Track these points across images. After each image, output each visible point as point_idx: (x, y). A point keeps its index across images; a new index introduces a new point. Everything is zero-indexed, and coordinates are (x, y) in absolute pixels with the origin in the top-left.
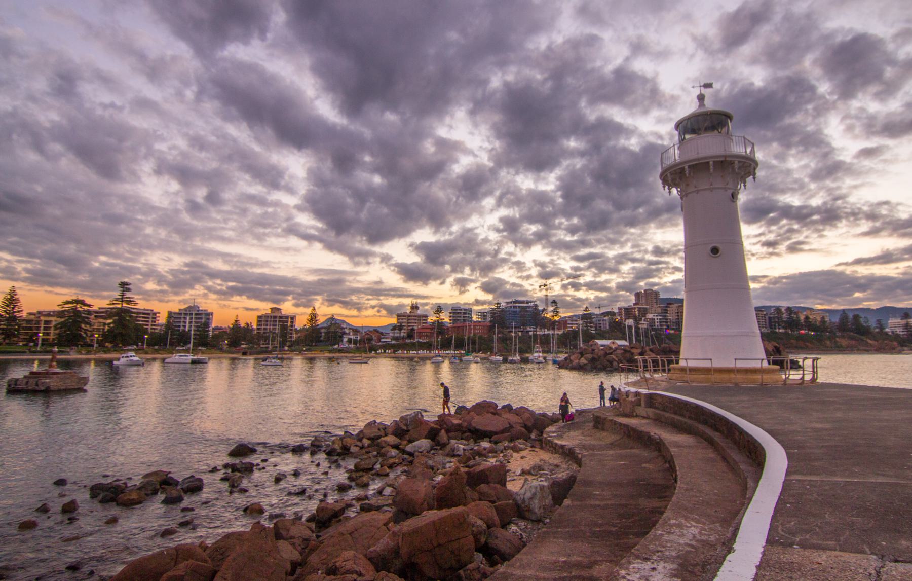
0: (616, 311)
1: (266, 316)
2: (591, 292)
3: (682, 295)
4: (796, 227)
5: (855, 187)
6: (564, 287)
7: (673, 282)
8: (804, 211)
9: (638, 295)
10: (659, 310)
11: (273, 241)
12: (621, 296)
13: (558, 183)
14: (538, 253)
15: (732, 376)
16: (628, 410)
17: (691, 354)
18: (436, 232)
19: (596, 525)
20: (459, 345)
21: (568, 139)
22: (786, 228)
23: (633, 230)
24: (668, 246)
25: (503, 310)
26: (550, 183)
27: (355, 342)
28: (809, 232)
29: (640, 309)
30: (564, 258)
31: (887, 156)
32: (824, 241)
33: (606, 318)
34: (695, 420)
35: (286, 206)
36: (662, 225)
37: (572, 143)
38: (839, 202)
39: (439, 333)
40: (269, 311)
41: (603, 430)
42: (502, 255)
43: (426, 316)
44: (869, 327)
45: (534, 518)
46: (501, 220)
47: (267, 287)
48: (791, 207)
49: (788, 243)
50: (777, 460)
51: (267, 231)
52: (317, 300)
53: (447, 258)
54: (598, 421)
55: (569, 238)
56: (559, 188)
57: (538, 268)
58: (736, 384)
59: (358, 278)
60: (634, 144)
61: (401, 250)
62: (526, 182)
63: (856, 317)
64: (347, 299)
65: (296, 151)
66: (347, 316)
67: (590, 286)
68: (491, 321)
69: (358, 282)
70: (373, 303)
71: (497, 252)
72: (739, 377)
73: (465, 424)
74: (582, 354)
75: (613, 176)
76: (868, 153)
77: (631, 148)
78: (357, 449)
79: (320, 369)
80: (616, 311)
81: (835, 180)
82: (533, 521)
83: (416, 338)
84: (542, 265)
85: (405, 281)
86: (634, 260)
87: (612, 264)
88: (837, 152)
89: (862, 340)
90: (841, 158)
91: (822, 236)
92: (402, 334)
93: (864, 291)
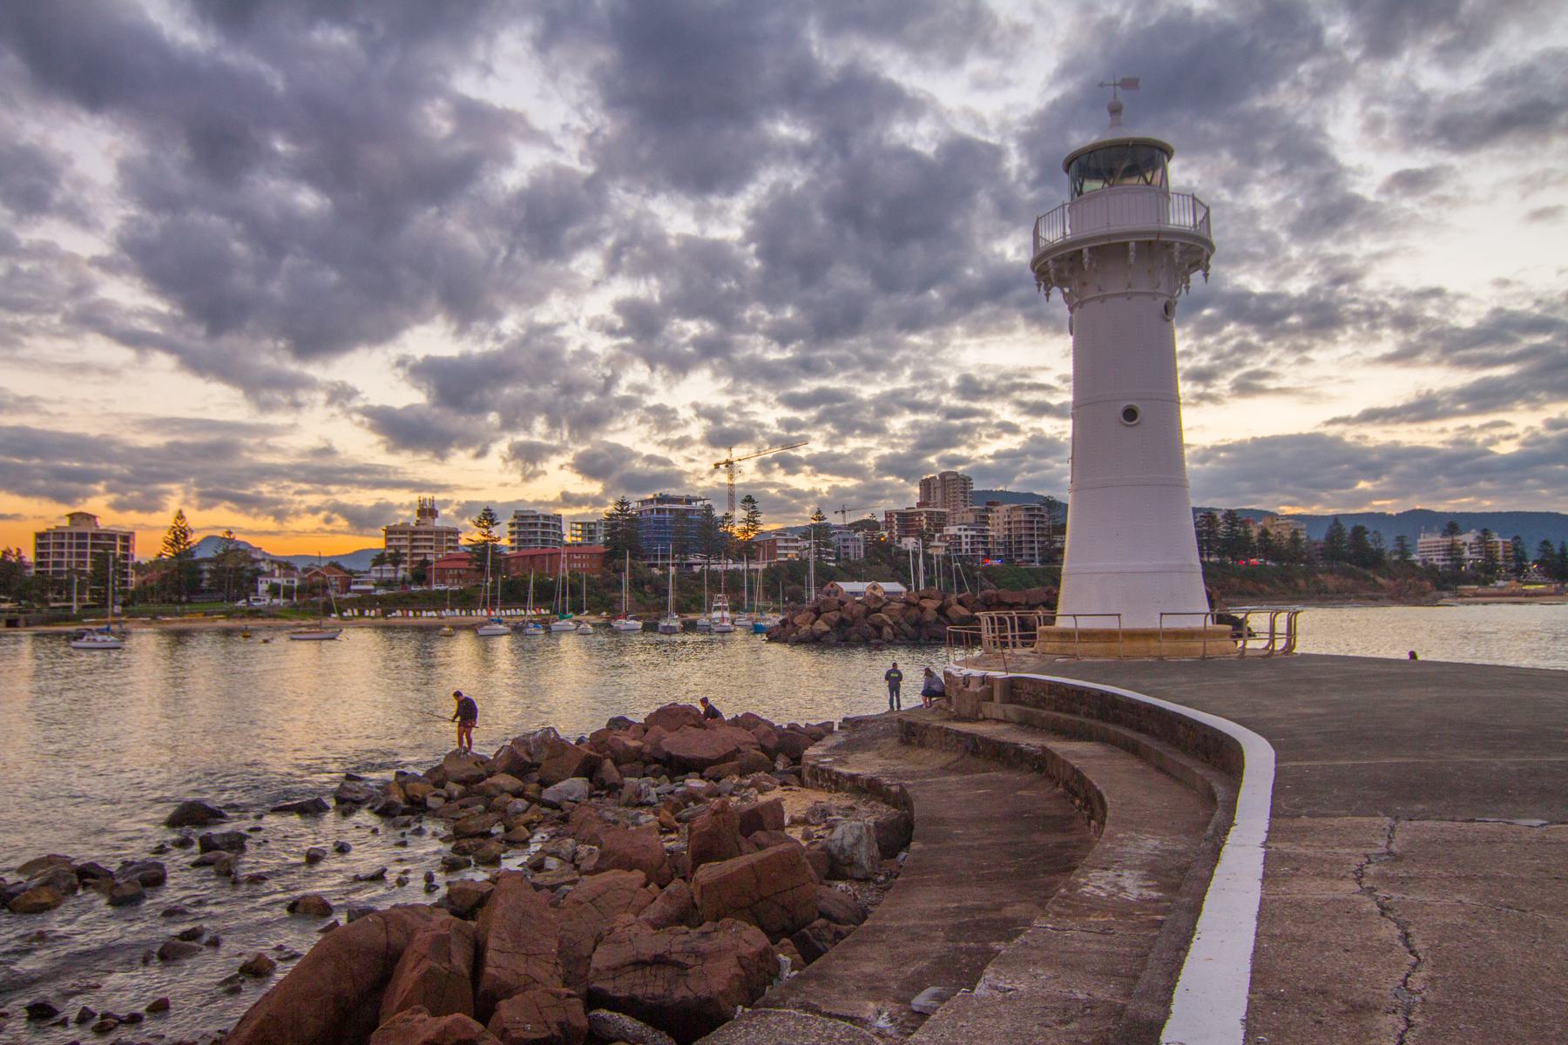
0: (881, 519)
1: (59, 533)
2: (822, 476)
3: (1065, 496)
4: (1254, 339)
5: (1379, 256)
6: (764, 466)
7: (998, 455)
8: (1274, 306)
9: (926, 485)
10: (971, 518)
11: (40, 346)
12: (886, 485)
13: (751, 223)
14: (702, 388)
15: (1153, 644)
16: (966, 710)
17: (1081, 604)
18: (461, 332)
19: (982, 868)
20: (545, 594)
21: (772, 116)
22: (1233, 342)
23: (915, 339)
24: (990, 377)
25: (633, 519)
26: (730, 222)
27: (289, 593)
28: (1281, 350)
29: (930, 515)
30: (764, 401)
31: (1448, 190)
32: (1309, 372)
33: (860, 535)
34: (1099, 718)
35: (70, 260)
36: (978, 330)
37: (785, 129)
38: (1343, 288)
39: (496, 571)
40: (66, 523)
41: (922, 745)
42: (621, 391)
43: (456, 532)
44: (1380, 552)
45: (859, 874)
46: (623, 307)
47: (36, 461)
48: (1249, 295)
49: (1235, 374)
50: (1259, 756)
51: (22, 319)
52: (170, 493)
53: (488, 394)
54: (909, 732)
55: (774, 355)
56: (751, 236)
57: (705, 422)
58: (1161, 658)
59: (272, 441)
60: (920, 137)
61: (377, 374)
62: (675, 219)
63: (1358, 532)
64: (250, 492)
65: (84, 116)
66: (250, 533)
67: (821, 464)
68: (607, 544)
69: (272, 449)
70: (314, 500)
71: (610, 382)
72: (1166, 645)
73: (647, 749)
74: (818, 613)
75: (875, 210)
76: (1409, 181)
77: (916, 146)
78: (440, 801)
79: (204, 656)
80: (881, 519)
81: (1343, 239)
82: (859, 880)
83: (426, 582)
84: (714, 415)
85: (391, 450)
86: (916, 407)
87: (867, 417)
88: (1350, 177)
89: (1366, 578)
90: (1358, 190)
91: (1304, 361)
92: (401, 574)
93: (1376, 477)
